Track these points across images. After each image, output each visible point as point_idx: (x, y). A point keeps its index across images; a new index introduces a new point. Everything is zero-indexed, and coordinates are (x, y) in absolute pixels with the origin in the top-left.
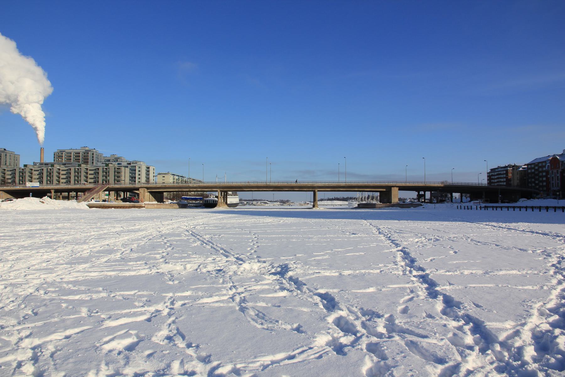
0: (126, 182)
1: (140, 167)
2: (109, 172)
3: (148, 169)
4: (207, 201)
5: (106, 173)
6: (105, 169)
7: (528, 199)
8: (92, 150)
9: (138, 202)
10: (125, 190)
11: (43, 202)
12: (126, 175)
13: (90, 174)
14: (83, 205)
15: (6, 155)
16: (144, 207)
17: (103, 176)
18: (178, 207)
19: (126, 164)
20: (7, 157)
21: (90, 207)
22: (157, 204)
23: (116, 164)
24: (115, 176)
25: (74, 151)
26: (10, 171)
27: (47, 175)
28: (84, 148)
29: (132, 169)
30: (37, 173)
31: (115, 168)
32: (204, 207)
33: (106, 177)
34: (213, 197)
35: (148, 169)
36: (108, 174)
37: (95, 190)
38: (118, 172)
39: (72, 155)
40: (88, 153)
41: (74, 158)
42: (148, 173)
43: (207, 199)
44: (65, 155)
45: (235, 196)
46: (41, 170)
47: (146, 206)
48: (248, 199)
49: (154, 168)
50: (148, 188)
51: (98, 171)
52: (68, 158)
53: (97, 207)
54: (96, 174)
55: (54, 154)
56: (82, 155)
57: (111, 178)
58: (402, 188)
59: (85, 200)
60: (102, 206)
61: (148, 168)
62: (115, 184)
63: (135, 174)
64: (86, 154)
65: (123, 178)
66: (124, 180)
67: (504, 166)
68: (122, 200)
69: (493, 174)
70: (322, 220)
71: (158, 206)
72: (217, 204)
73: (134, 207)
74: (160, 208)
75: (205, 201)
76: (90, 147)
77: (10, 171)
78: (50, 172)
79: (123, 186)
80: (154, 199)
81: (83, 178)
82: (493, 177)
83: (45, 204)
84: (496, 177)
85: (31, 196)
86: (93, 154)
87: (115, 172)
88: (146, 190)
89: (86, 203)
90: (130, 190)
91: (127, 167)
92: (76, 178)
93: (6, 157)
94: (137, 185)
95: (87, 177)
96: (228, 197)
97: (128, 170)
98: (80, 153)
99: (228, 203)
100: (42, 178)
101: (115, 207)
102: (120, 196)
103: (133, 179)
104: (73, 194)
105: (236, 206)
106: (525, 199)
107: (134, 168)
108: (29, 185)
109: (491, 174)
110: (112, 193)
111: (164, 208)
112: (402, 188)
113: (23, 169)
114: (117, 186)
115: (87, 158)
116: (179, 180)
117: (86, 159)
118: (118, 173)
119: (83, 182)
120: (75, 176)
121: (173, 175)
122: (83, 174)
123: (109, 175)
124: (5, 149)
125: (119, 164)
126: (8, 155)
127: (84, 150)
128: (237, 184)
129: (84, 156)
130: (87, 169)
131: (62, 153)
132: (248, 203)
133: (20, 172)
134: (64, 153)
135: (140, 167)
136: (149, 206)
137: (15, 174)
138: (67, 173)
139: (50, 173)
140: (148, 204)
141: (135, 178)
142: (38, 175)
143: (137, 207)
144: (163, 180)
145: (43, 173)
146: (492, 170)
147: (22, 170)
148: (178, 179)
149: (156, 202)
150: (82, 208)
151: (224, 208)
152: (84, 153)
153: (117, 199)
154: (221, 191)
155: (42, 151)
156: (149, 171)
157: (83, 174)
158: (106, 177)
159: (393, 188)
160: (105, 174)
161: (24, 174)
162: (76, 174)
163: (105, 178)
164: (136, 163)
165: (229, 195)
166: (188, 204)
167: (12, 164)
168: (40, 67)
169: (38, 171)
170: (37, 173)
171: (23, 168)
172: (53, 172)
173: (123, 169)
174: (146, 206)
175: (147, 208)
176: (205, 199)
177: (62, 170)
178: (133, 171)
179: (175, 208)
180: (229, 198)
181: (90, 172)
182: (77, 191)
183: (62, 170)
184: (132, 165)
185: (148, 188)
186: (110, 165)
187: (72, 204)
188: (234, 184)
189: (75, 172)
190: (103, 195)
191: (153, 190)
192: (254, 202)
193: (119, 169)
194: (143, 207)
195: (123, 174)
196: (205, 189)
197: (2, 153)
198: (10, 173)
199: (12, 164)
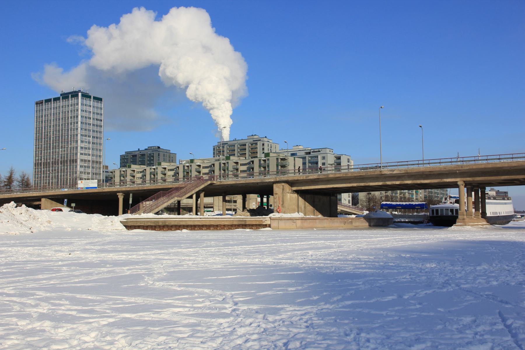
1: (324, 158)
3: (338, 161)
4: (437, 211)
8: (262, 139)
15: (159, 155)
16: (270, 226)
18: (367, 224)
19: (304, 154)
20: (160, 157)
22: (302, 219)
25: (239, 142)
26: (141, 172)
28: (252, 137)
29: (312, 161)
30: (172, 173)
32: (430, 224)
34: (451, 203)
35: (338, 161)
39: (236, 148)
40: (256, 144)
41: (238, 152)
43: (438, 206)
44: (227, 148)
45: (504, 199)
47: (274, 224)
49: (349, 157)
50: (291, 183)
51: (252, 166)
55: (214, 149)
56: (249, 146)
60: (160, 224)
61: (339, 158)
64: (254, 145)
72: (457, 217)
74: (312, 228)
75: (433, 211)
76: (260, 134)
77: (141, 172)
78: (187, 171)
85: (65, 204)
86: (263, 145)
87: (277, 166)
88: (287, 186)
93: (159, 158)
96: (487, 201)
98: (245, 145)
99: (488, 215)
105: (508, 222)
107: (314, 160)
117: (254, 153)
124: (159, 147)
126: (161, 154)
127: (251, 140)
128: (515, 160)
129: (252, 149)
133: (151, 173)
134: (225, 146)
135: (324, 158)
136: (282, 224)
139: (188, 173)
142: (173, 176)
149: (320, 216)
152: (252, 145)
154: (466, 184)
160: (262, 169)
164: (319, 151)
165: (489, 198)
166: (392, 219)
168: (170, 9)
172: (191, 171)
174: (274, 224)
175: (278, 228)
176: (432, 206)
179: (357, 228)
180: (491, 203)
184: (312, 154)
185: (291, 183)
188: (506, 163)
191: (303, 188)
194: (265, 226)
196: (424, 179)
197: (154, 152)
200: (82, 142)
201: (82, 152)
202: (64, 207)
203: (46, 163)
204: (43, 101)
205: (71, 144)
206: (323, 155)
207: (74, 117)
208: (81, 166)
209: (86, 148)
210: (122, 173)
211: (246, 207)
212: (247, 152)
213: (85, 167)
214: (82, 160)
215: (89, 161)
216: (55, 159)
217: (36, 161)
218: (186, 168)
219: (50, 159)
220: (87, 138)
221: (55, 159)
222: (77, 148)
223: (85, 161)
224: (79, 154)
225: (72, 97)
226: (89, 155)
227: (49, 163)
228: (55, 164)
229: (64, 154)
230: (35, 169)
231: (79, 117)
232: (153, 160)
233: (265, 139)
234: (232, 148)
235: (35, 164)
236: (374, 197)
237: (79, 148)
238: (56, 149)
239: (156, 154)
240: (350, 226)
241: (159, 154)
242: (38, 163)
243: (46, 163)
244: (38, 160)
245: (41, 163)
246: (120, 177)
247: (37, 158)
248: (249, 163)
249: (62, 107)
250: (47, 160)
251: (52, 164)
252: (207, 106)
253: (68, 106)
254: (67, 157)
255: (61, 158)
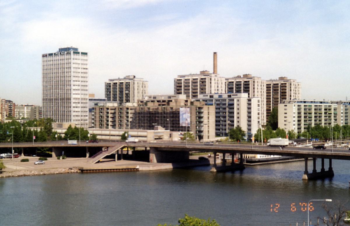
1: (238, 101)
135: (238, 101)
204: (47, 54)
206: (238, 99)
211: (281, 126)
216: (56, 97)
217: (43, 97)
230: (43, 103)
235: (43, 99)
238: (56, 89)
240: (144, 128)
241: (134, 83)
252: (135, 109)
255: (61, 96)
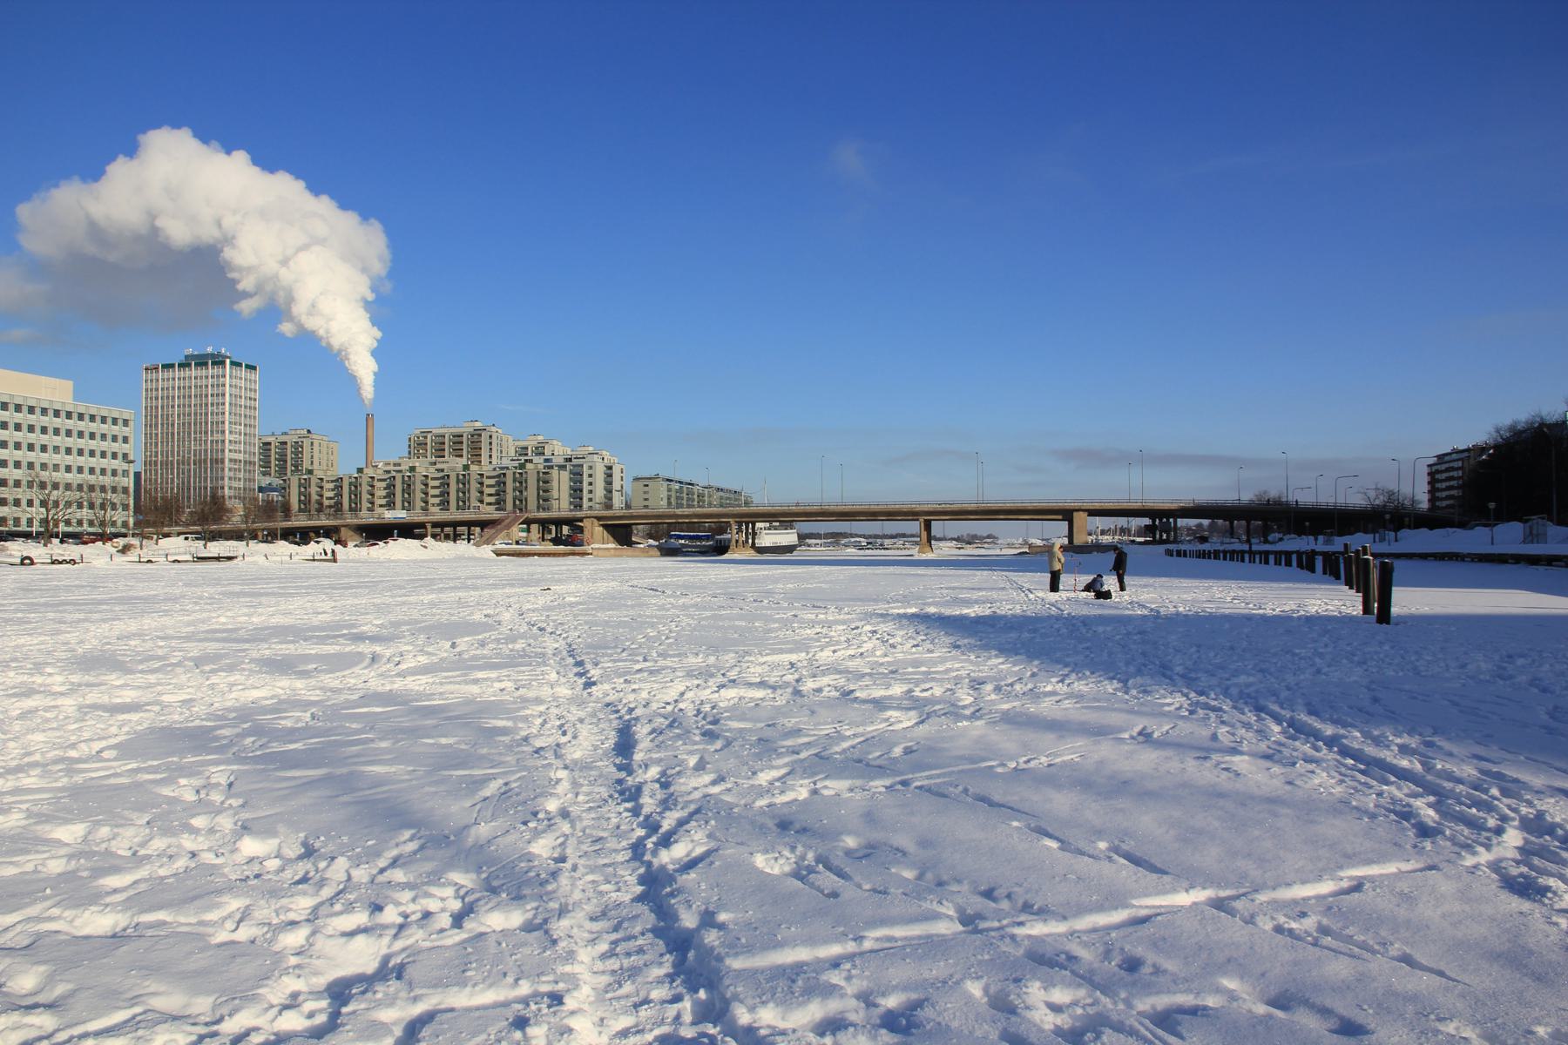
0: (561, 505)
2: (526, 481)
5: (521, 483)
6: (518, 476)
7: (1299, 536)
8: (488, 428)
9: (582, 545)
10: (559, 522)
11: (425, 547)
12: (561, 484)
13: (488, 486)
14: (486, 551)
17: (514, 490)
21: (498, 555)
23: (538, 460)
24: (538, 489)
26: (332, 481)
27: (403, 490)
30: (384, 484)
31: (538, 472)
33: (521, 492)
36: (524, 485)
37: (504, 524)
38: (544, 481)
40: (480, 435)
42: (609, 479)
46: (390, 478)
47: (595, 553)
48: (894, 533)
50: (599, 518)
52: (438, 447)
53: (508, 555)
54: (499, 486)
57: (531, 494)
58: (1093, 513)
59: (488, 542)
61: (610, 468)
62: (538, 511)
63: (581, 482)
65: (555, 494)
66: (559, 499)
67: (1465, 447)
68: (551, 540)
69: (1439, 470)
70: (840, 567)
71: (618, 553)
73: (574, 554)
74: (621, 556)
77: (332, 481)
79: (554, 514)
80: (611, 539)
81: (474, 494)
82: (1438, 476)
83: (429, 550)
84: (1444, 476)
86: (491, 437)
87: (538, 481)
88: (595, 521)
89: (490, 547)
90: (569, 522)
91: (565, 467)
92: (461, 495)
94: (579, 514)
95: (481, 493)
97: (565, 475)
98: (462, 436)
100: (394, 495)
101: (540, 555)
102: (550, 532)
103: (576, 492)
104: (448, 530)
106: (1293, 536)
107: (577, 470)
108: (390, 515)
109: (1434, 468)
110: (534, 527)
111: (628, 556)
112: (1093, 513)
113: (356, 478)
114: (543, 515)
115: (477, 445)
116: (682, 493)
118: (544, 482)
119: (474, 503)
120: (458, 492)
121: (668, 480)
122: (474, 486)
123: (526, 487)
125: (547, 460)
129: (472, 442)
130: (482, 475)
131: (426, 437)
132: (870, 543)
133: (350, 484)
134: (429, 436)
135: (591, 468)
136: (601, 553)
137: (342, 487)
138: (442, 485)
140: (599, 549)
141: (581, 491)
142: (385, 489)
143: (578, 554)
144: (645, 493)
145: (394, 486)
146: (1439, 457)
147: (354, 480)
148: (680, 491)
150: (485, 556)
151: (749, 554)
152: (472, 436)
153: (543, 540)
155: (370, 423)
156: (610, 476)
157: (474, 486)
158: (521, 492)
159: (1075, 514)
160: (518, 484)
161: (359, 489)
162: (461, 486)
163: (518, 493)
167: (324, 463)
169: (384, 480)
170: (384, 484)
171: (356, 475)
172: (414, 484)
173: (555, 472)
174: (595, 553)
175: (597, 556)
177: (432, 479)
178: (577, 475)
181: (487, 482)
182: (469, 524)
183: (432, 479)
184: (575, 462)
185: (599, 518)
186: (529, 466)
187: (462, 547)
189: (458, 482)
190: (517, 532)
192: (887, 542)
193: (547, 473)
194: (588, 554)
195: (555, 484)
197: (304, 440)
198: (331, 486)
199: (324, 463)
200: (231, 432)
201: (231, 448)
202: (1340, 584)
203: (167, 461)
205: (212, 435)
206: (590, 464)
207: (218, 395)
208: (230, 469)
209: (236, 442)
210: (303, 481)
212: (464, 446)
213: (235, 469)
214: (231, 460)
215: (240, 461)
216: (184, 456)
218: (406, 479)
219: (173, 456)
220: (238, 427)
221: (184, 456)
222: (223, 441)
223: (235, 461)
224: (227, 451)
225: (213, 363)
226: (240, 452)
227: (172, 462)
228: (184, 464)
229: (200, 450)
231: (227, 395)
232: (302, 453)
233: (494, 429)
234: (441, 439)
236: (343, 353)
237: (227, 442)
239: (306, 443)
242: (151, 461)
243: (167, 461)
244: (151, 456)
245: (156, 462)
246: (299, 487)
247: (149, 453)
248: (499, 476)
249: (196, 378)
250: (167, 457)
251: (178, 464)
253: (207, 377)
254: (206, 455)
255: (195, 455)
